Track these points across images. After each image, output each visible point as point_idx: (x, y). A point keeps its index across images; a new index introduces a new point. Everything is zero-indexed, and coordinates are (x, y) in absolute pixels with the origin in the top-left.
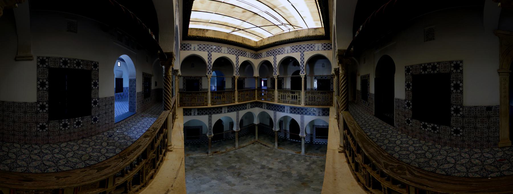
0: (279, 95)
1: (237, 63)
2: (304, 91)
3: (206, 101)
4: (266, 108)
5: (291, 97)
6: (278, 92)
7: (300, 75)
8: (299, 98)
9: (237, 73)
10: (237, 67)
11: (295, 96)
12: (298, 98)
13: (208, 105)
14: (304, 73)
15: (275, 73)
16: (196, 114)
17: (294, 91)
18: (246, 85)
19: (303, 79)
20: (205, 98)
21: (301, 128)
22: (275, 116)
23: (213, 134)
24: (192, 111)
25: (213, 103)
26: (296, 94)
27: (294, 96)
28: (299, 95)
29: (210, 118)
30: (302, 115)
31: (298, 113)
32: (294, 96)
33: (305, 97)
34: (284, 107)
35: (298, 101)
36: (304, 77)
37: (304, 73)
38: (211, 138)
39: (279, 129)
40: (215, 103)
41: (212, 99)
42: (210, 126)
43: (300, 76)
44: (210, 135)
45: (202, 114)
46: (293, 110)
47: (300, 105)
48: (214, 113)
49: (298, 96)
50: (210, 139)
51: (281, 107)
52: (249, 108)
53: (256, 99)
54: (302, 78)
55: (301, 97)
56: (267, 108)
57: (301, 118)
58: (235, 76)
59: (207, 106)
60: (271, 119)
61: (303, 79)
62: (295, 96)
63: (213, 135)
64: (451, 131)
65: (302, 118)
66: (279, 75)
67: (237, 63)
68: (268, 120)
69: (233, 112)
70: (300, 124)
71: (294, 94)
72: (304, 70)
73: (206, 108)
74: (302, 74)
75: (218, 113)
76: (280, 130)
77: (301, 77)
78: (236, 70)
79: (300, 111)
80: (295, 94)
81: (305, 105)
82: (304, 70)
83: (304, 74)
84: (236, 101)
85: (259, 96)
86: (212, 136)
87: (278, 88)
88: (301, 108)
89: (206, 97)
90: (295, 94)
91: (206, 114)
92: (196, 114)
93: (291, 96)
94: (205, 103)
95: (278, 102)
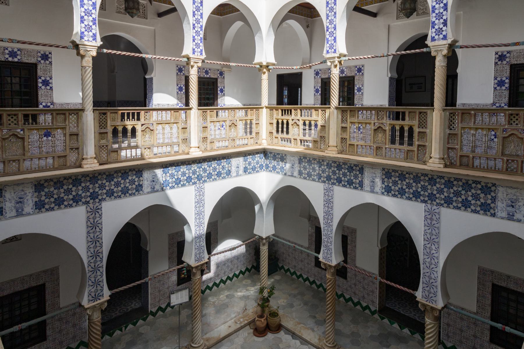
0: (344, 125)
1: (198, 9)
2: (444, 110)
3: (75, 146)
4: (296, 174)
5: (388, 133)
6: (340, 117)
7: (427, 46)
8: (423, 135)
9: (197, 45)
10: (198, 21)
11: (406, 128)
12: (416, 135)
13: (84, 162)
14: (445, 38)
15: (331, 47)
16: (29, 207)
17: (401, 109)
18: (366, 90)
19: (440, 64)
20: (71, 135)
21: (424, 263)
22: (329, 202)
23: (110, 288)
24: (8, 195)
25: (104, 155)
26: (407, 123)
27: (402, 129)
28: (423, 123)
29: (94, 218)
30: (429, 206)
31: (416, 196)
32: (402, 129)
33: (448, 131)
34: (361, 171)
35: (416, 149)
36: (445, 52)
37: (445, 38)
38: (103, 312)
39: (342, 258)
40: (114, 155)
41: (103, 139)
42: (96, 255)
43: (430, 53)
44: (95, 298)
45: (59, 203)
46: (395, 183)
47: (425, 163)
48: (111, 194)
49: (416, 130)
50: (97, 317)
51: (351, 169)
52: (238, 175)
53: (264, 142)
54: (434, 58)
55: (428, 131)
56: (300, 173)
57: (426, 218)
58: (191, 55)
59: (80, 166)
60: (313, 219)
61: (440, 64)
62: (406, 128)
63: (107, 294)
64: (221, 78)
65: (431, 219)
66: (345, 52)
67: (198, 9)
68: (308, 229)
69: (183, 185)
70: (422, 243)
71: (401, 122)
72: (445, 24)
73: (76, 175)
74: (436, 43)
75: (125, 192)
76: (345, 261)
77: (433, 54)
78: (192, 33)
79: (87, 189)
80: (403, 119)
81: (446, 166)
82: (445, 24)
83: (444, 42)
84: (192, 145)
85: (274, 131)
86: (102, 300)
87: (201, 104)
88: (426, 175)
89: (75, 130)
90: (403, 119)
91: (77, 200)
92: (29, 207)
93: (387, 128)
94: (72, 157)
95: (341, 152)
